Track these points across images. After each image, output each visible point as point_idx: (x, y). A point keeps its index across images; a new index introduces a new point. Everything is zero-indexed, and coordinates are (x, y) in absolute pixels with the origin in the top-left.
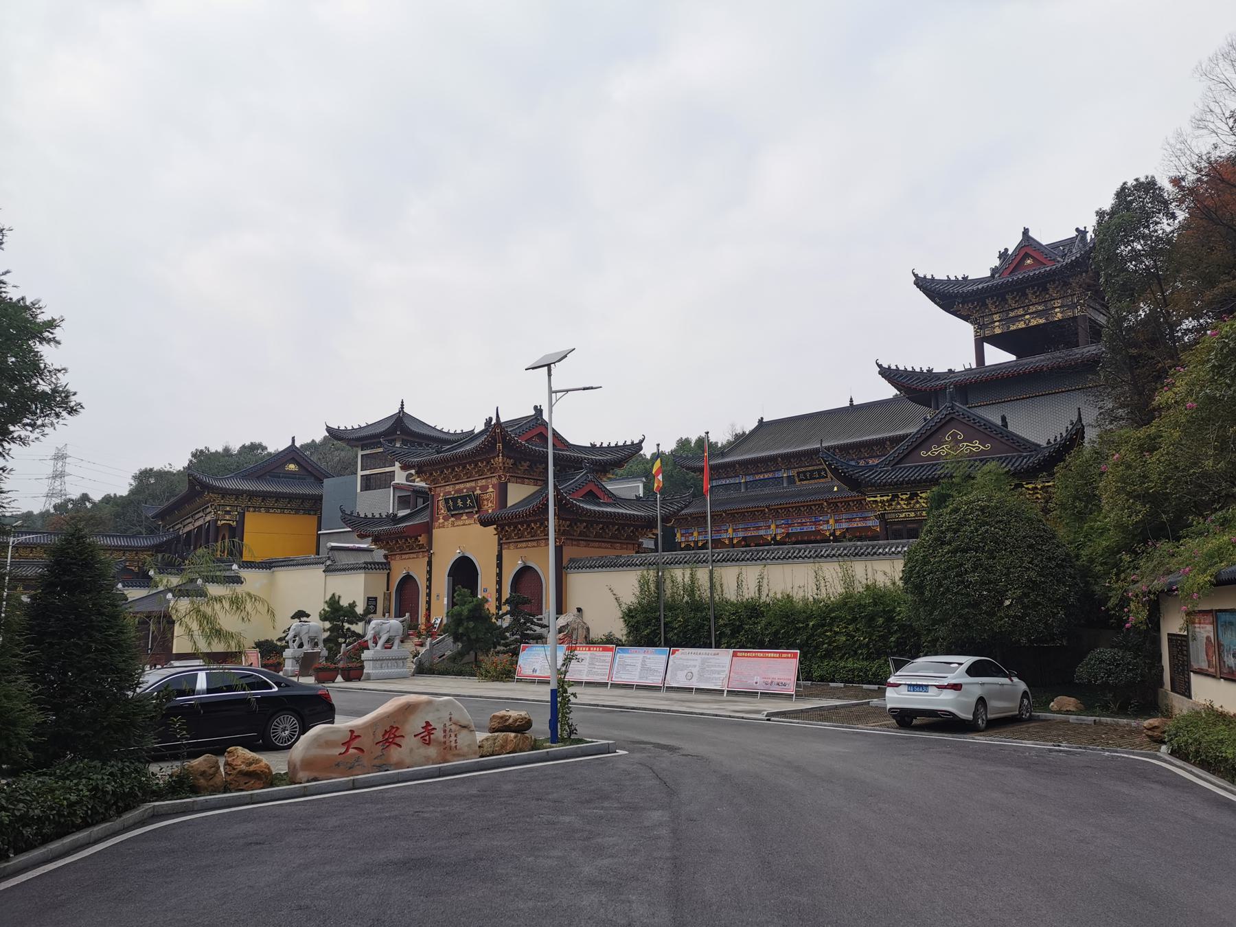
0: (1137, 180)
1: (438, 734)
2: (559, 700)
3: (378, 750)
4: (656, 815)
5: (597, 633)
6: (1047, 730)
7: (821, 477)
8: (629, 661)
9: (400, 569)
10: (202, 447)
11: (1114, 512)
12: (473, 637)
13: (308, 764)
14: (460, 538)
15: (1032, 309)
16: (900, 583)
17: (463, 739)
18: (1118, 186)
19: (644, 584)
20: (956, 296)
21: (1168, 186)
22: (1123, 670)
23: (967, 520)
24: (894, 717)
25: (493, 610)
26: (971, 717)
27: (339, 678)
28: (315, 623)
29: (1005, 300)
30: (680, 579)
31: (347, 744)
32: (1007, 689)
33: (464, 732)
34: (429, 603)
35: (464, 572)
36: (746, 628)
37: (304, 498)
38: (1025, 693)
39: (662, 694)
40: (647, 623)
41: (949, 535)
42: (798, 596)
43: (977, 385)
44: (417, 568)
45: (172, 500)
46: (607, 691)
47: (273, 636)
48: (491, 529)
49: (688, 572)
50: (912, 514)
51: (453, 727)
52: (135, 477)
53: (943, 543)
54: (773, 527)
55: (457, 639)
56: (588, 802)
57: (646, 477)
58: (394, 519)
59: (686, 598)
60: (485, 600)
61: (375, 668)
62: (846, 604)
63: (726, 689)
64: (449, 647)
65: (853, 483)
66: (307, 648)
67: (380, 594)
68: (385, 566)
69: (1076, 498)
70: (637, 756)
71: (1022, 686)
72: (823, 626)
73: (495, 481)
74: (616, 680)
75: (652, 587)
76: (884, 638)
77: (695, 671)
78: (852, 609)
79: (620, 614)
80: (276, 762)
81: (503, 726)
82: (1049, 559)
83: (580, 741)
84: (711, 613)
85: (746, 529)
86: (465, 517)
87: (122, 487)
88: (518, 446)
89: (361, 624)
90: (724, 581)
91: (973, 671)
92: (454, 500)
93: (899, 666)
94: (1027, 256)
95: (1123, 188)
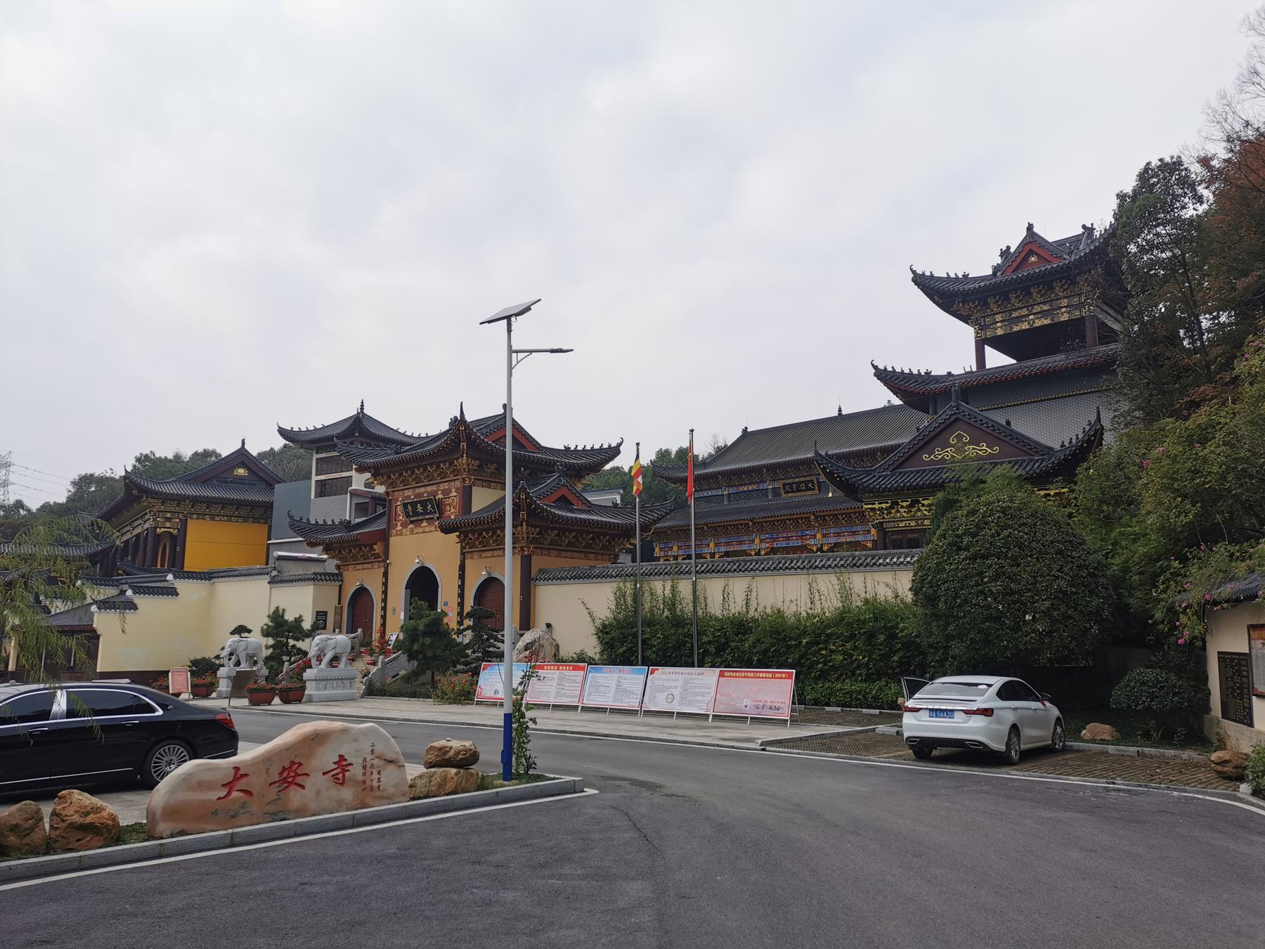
0: (1161, 160)
1: (356, 772)
2: (514, 728)
3: (272, 793)
4: (636, 889)
5: (567, 651)
6: (1088, 763)
7: (808, 489)
8: (602, 682)
11: (1154, 513)
12: (429, 654)
13: (172, 812)
14: (421, 547)
15: (1037, 309)
16: (909, 597)
17: (389, 777)
18: (1142, 166)
19: (620, 597)
20: (957, 294)
21: (1196, 170)
22: (1168, 694)
23: (987, 523)
24: (911, 747)
25: (453, 625)
26: (1003, 748)
27: (277, 700)
28: (258, 642)
29: (1008, 299)
30: (659, 592)
31: (229, 785)
32: (1039, 715)
33: (391, 768)
34: (384, 617)
35: (423, 584)
36: (734, 645)
37: (252, 505)
38: (1058, 718)
39: (640, 719)
40: (623, 639)
41: (966, 540)
42: (789, 610)
43: (978, 388)
44: (370, 579)
46: (578, 715)
47: (210, 654)
48: (453, 536)
49: (669, 585)
50: (913, 523)
51: (376, 762)
52: (74, 483)
53: (960, 549)
54: (757, 541)
55: (411, 656)
56: (543, 866)
57: (624, 489)
58: (347, 526)
59: (667, 613)
60: (444, 614)
61: (318, 689)
62: (843, 619)
63: (711, 713)
64: (404, 666)
65: (851, 490)
66: (244, 667)
67: (330, 607)
68: (337, 577)
69: (1102, 502)
70: (610, 796)
71: (1055, 712)
72: (818, 643)
73: (458, 484)
74: (588, 702)
75: (629, 600)
76: (886, 657)
77: (676, 693)
78: (849, 625)
79: (593, 630)
80: (126, 809)
81: (442, 760)
82: (1080, 567)
83: (540, 778)
84: (694, 630)
85: (728, 544)
87: (60, 494)
89: (308, 641)
90: (709, 595)
91: (1004, 693)
92: (414, 504)
93: (914, 688)
94: (1031, 253)
95: (1147, 168)
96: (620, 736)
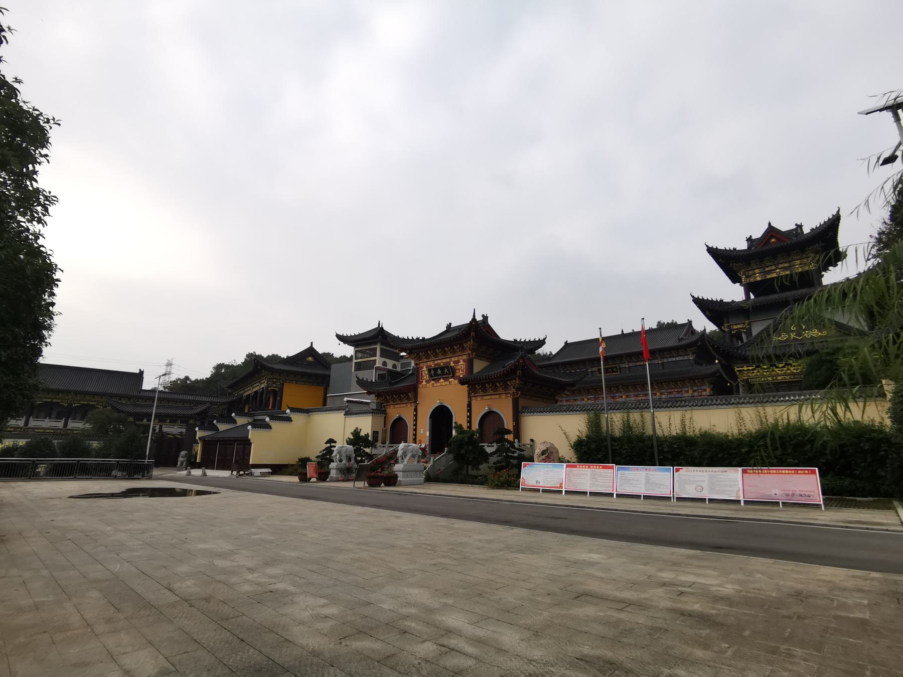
9: (394, 412)
10: (252, 352)
15: (781, 266)
44: (405, 412)
45: (235, 380)
50: (770, 379)
67: (380, 429)
73: (465, 357)
86: (442, 380)
88: (476, 335)
92: (435, 370)
96: (687, 515)
